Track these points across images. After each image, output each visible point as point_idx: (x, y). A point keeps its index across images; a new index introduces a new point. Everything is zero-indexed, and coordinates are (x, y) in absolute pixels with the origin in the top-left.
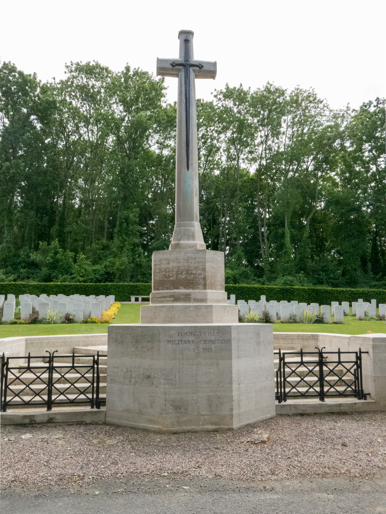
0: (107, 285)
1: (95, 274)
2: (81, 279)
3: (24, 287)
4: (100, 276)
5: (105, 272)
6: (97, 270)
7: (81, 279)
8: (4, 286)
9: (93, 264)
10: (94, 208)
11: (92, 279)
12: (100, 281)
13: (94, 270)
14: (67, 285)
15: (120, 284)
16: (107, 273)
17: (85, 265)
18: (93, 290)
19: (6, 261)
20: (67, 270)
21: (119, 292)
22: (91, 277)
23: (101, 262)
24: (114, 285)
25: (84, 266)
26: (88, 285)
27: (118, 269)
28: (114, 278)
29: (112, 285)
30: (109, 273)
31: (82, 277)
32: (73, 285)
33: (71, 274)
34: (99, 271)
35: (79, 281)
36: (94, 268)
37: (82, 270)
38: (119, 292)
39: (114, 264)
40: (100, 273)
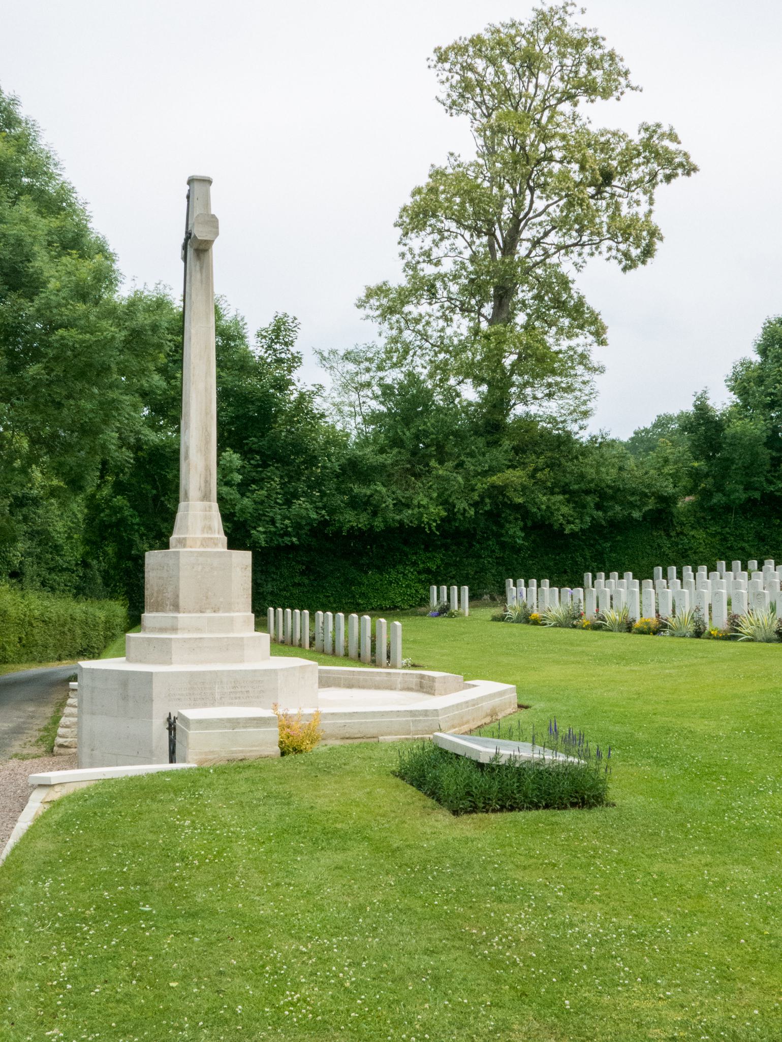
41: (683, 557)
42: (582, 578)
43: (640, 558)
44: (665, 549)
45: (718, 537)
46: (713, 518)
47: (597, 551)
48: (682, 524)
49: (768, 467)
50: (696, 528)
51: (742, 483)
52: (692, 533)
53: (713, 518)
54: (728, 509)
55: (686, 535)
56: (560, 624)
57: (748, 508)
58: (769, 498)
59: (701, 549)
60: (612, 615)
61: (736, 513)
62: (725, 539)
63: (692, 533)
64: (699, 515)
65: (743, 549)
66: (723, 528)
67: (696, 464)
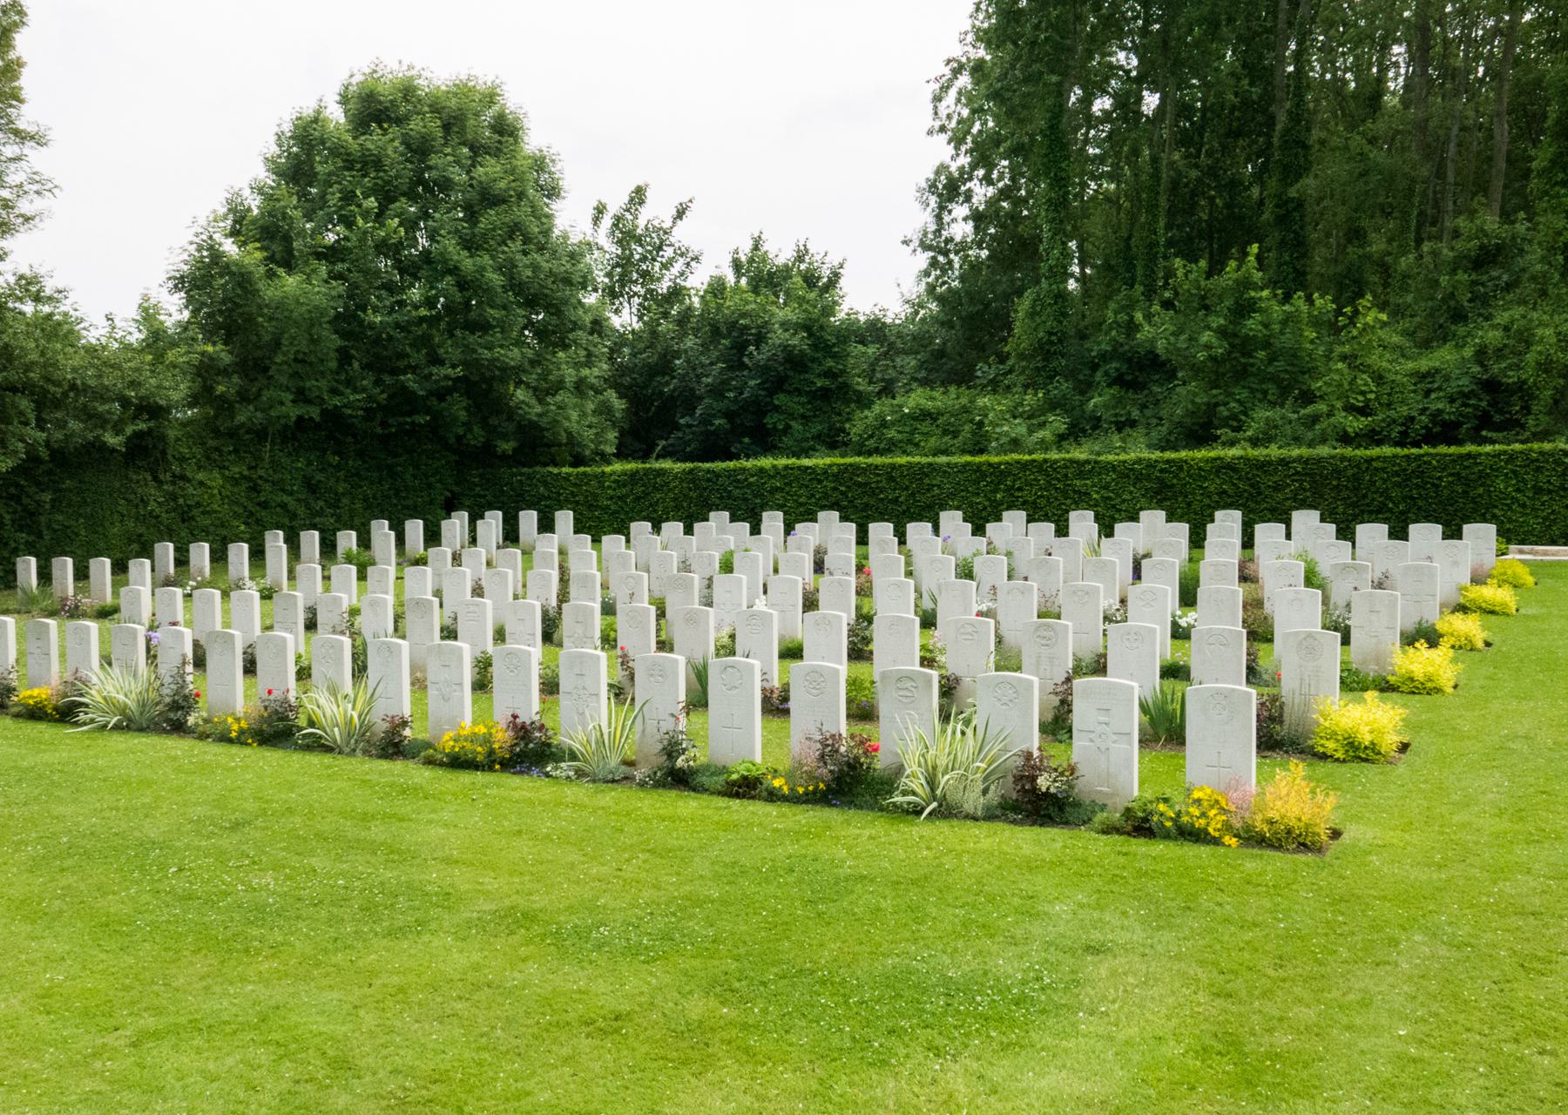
0: (1469, 456)
1: (1428, 393)
2: (1354, 424)
3: (1081, 475)
4: (1452, 401)
5: (1479, 382)
6: (1437, 371)
7: (1354, 424)
8: (1002, 472)
9: (1426, 345)
10: (1293, 47)
11: (1412, 419)
12: (1446, 432)
13: (1423, 377)
14: (1270, 463)
15: (1547, 446)
16: (1491, 386)
17: (1383, 354)
18: (1398, 485)
19: (1048, 356)
20: (1293, 384)
21: (1538, 490)
22: (1404, 411)
23: (1461, 330)
24: (1512, 457)
25: (1378, 360)
26: (1369, 460)
27: (1545, 366)
28: (1527, 409)
29: (1498, 455)
30: (1500, 384)
31: (1364, 411)
32: (1299, 459)
33: (1308, 398)
34: (1447, 379)
35: (1345, 439)
36: (1424, 364)
37: (1364, 379)
38: (1538, 490)
39: (1525, 339)
40: (1452, 387)
41: (183, 521)
42: (13, 572)
43: (107, 524)
44: (152, 506)
45: (245, 485)
46: (236, 451)
47: (25, 509)
48: (182, 460)
49: (333, 364)
50: (205, 468)
51: (288, 389)
52: (200, 476)
53: (236, 451)
54: (261, 435)
55: (189, 481)
56: (129, 724)
57: (296, 434)
58: (334, 422)
59: (215, 507)
60: (330, 706)
61: (273, 443)
62: (255, 489)
63: (200, 476)
64: (211, 443)
65: (283, 506)
66: (250, 468)
67: (210, 349)
